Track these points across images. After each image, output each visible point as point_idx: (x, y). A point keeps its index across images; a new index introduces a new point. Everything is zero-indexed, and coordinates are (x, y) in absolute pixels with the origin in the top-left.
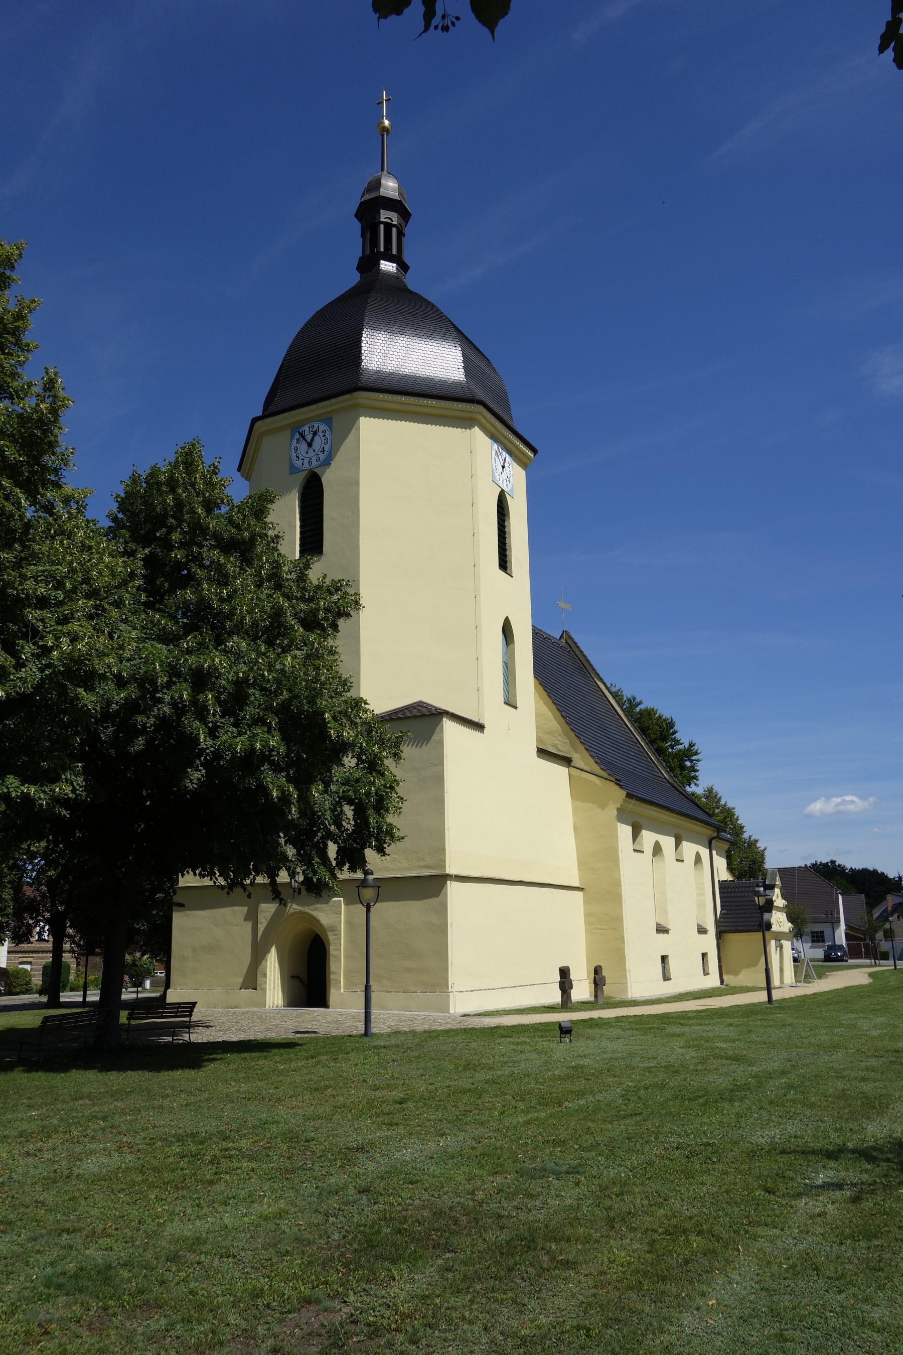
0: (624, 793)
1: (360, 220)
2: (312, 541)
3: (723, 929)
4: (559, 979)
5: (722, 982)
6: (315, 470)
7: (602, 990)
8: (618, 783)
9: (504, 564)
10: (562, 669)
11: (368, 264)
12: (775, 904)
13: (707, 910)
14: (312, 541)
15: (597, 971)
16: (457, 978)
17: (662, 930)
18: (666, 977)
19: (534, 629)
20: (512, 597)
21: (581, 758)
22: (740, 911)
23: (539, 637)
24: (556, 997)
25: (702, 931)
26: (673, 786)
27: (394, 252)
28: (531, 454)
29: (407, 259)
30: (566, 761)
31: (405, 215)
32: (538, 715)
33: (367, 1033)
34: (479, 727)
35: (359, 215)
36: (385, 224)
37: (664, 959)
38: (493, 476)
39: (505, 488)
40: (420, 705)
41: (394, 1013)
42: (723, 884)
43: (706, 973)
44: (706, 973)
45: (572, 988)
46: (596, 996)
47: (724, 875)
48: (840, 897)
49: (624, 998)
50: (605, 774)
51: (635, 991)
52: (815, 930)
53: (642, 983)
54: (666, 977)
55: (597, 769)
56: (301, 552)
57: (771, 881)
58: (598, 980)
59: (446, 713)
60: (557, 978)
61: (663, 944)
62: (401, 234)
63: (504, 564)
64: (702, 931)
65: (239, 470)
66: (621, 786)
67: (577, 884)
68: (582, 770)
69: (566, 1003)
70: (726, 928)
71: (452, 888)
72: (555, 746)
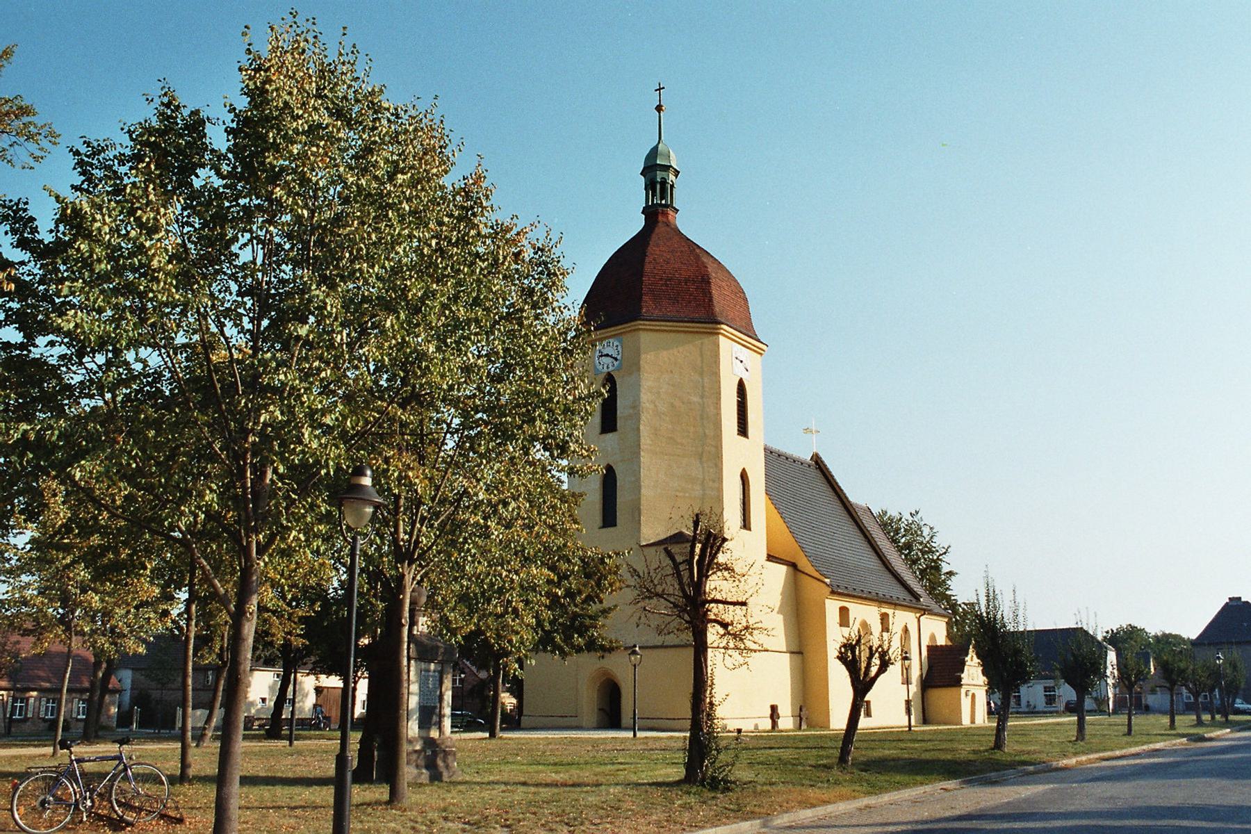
24: (767, 724)
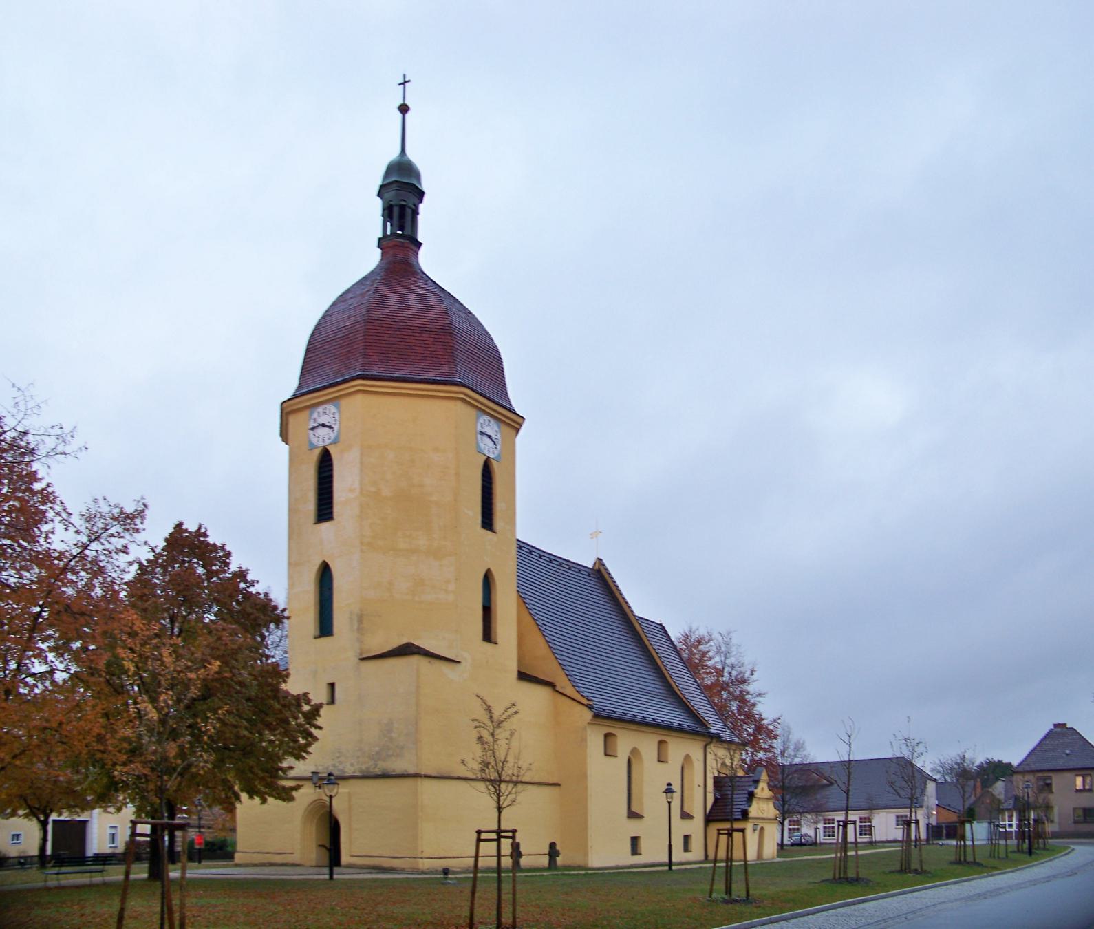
1: (381, 198)
5: (504, 856)
6: (328, 447)
9: (488, 636)
18: (635, 850)
24: (545, 861)
54: (635, 850)
60: (546, 850)
61: (634, 828)
63: (488, 636)
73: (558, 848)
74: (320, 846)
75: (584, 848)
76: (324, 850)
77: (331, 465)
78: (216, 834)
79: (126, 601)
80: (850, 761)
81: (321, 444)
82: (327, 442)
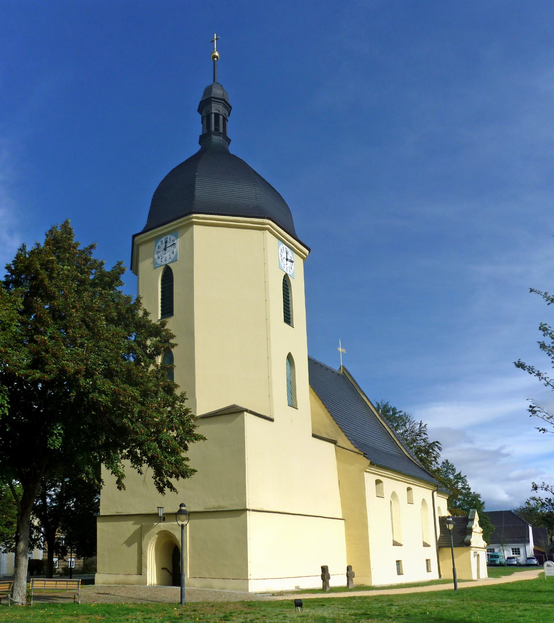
0: (369, 462)
1: (201, 113)
2: (168, 309)
3: (440, 545)
4: (321, 573)
5: (440, 576)
6: (169, 265)
7: (352, 580)
8: (365, 455)
9: (288, 319)
10: (333, 387)
11: (204, 139)
12: (474, 530)
13: (431, 534)
14: (168, 309)
15: (349, 568)
16: (253, 570)
17: (395, 544)
18: (399, 572)
19: (309, 359)
20: (295, 340)
21: (343, 441)
22: (453, 536)
23: (313, 364)
24: (318, 584)
25: (426, 545)
26: (410, 460)
27: (221, 130)
28: (307, 251)
29: (229, 135)
30: (334, 442)
31: (228, 107)
32: (313, 414)
33: (181, 603)
34: (272, 420)
35: (200, 110)
36: (216, 114)
37: (398, 562)
38: (280, 264)
39: (288, 273)
40: (234, 406)
41: (223, 588)
42: (443, 520)
43: (428, 570)
44: (428, 570)
45: (329, 578)
46: (348, 584)
47: (445, 513)
48: (530, 528)
49: (367, 584)
50: (357, 450)
51: (376, 581)
52: (514, 547)
53: (381, 575)
54: (399, 572)
55: (352, 447)
56: (162, 314)
57: (471, 516)
58: (350, 574)
59: (247, 411)
60: (320, 573)
61: (397, 553)
62: (225, 120)
63: (288, 319)
64: (426, 545)
65: (131, 269)
66: (367, 458)
67: (341, 518)
68: (343, 448)
69: (325, 588)
70: (443, 545)
71: (250, 515)
72: (328, 434)
73: (353, 570)
74: (162, 568)
75: (368, 573)
76: (165, 571)
77: (172, 274)
78: (456, 612)
79: (107, 438)
80: (248, 580)
81: (164, 263)
82: (168, 261)
